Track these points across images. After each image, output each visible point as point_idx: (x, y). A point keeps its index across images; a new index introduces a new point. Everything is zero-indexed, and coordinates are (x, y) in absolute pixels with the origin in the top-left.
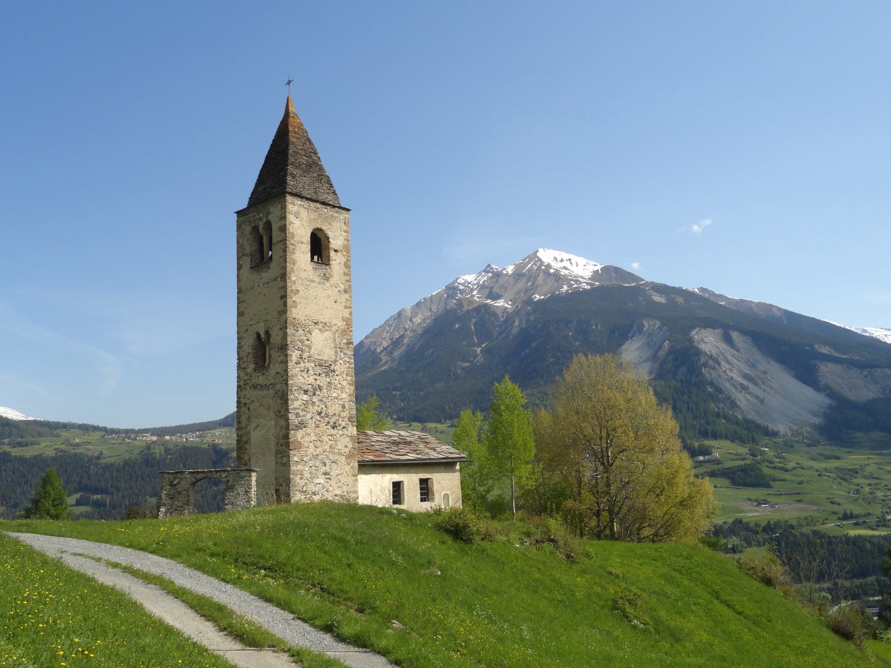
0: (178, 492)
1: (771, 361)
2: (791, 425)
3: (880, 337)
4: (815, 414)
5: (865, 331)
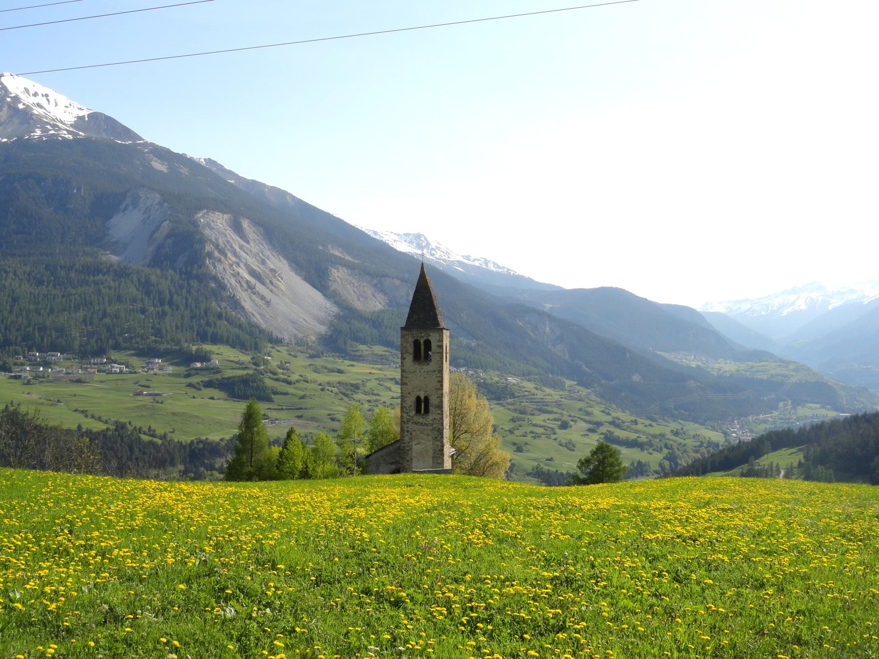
3: (389, 242)
4: (321, 322)
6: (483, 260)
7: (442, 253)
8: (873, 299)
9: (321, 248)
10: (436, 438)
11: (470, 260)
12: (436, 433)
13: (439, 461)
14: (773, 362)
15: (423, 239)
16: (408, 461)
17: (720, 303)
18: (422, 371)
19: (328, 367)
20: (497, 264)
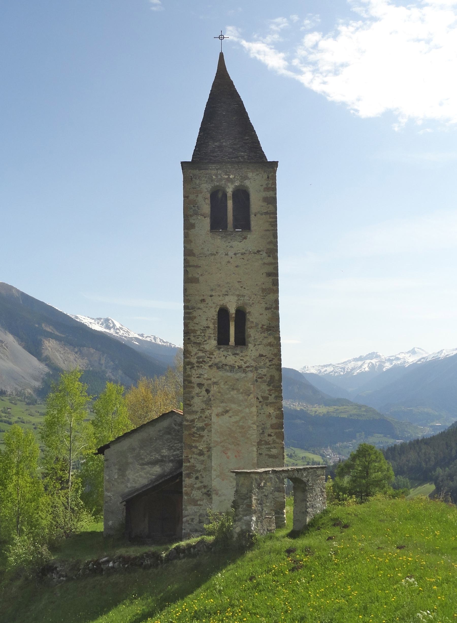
0: (265, 495)
1: (8, 333)
2: (17, 386)
3: (86, 324)
4: (36, 379)
5: (77, 317)
6: (153, 337)
7: (124, 332)
8: (411, 363)
9: (37, 326)
10: (265, 398)
11: (143, 337)
12: (264, 387)
13: (274, 451)
14: (351, 406)
15: (110, 322)
16: (201, 453)
17: (313, 367)
18: (231, 254)
19: (40, 412)
20: (162, 340)
